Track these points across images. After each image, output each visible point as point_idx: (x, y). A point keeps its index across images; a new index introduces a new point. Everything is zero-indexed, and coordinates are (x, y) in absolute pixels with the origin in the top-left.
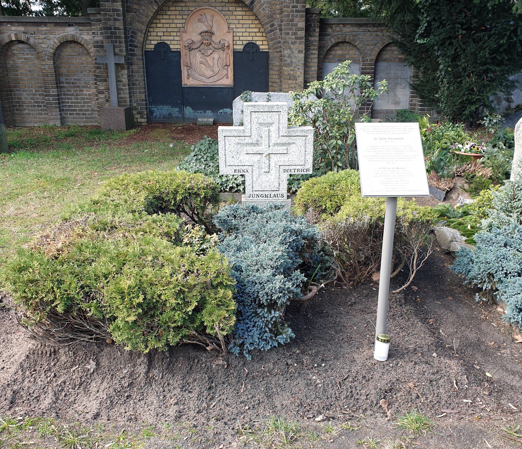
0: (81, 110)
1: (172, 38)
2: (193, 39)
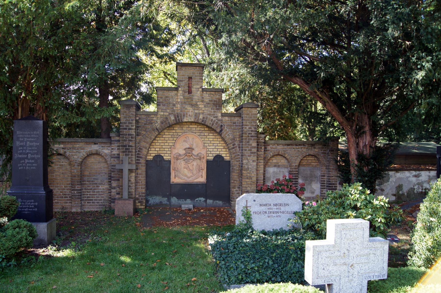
0: (96, 200)
1: (165, 152)
2: (180, 153)
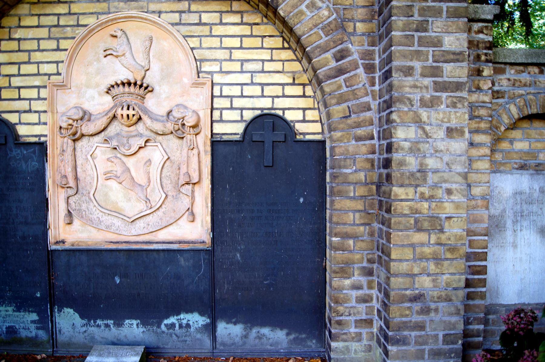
1: (23, 105)
